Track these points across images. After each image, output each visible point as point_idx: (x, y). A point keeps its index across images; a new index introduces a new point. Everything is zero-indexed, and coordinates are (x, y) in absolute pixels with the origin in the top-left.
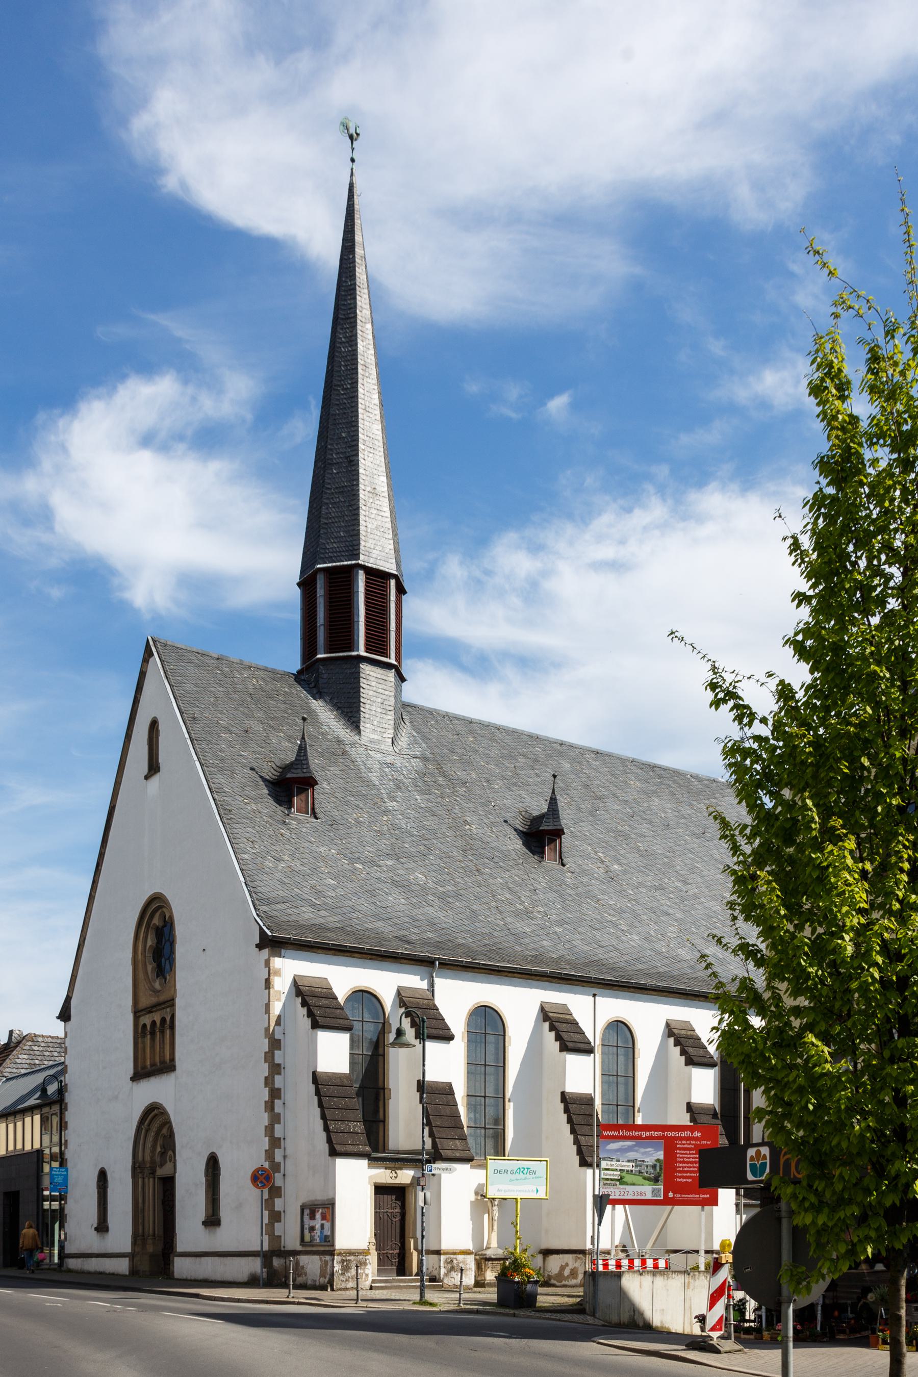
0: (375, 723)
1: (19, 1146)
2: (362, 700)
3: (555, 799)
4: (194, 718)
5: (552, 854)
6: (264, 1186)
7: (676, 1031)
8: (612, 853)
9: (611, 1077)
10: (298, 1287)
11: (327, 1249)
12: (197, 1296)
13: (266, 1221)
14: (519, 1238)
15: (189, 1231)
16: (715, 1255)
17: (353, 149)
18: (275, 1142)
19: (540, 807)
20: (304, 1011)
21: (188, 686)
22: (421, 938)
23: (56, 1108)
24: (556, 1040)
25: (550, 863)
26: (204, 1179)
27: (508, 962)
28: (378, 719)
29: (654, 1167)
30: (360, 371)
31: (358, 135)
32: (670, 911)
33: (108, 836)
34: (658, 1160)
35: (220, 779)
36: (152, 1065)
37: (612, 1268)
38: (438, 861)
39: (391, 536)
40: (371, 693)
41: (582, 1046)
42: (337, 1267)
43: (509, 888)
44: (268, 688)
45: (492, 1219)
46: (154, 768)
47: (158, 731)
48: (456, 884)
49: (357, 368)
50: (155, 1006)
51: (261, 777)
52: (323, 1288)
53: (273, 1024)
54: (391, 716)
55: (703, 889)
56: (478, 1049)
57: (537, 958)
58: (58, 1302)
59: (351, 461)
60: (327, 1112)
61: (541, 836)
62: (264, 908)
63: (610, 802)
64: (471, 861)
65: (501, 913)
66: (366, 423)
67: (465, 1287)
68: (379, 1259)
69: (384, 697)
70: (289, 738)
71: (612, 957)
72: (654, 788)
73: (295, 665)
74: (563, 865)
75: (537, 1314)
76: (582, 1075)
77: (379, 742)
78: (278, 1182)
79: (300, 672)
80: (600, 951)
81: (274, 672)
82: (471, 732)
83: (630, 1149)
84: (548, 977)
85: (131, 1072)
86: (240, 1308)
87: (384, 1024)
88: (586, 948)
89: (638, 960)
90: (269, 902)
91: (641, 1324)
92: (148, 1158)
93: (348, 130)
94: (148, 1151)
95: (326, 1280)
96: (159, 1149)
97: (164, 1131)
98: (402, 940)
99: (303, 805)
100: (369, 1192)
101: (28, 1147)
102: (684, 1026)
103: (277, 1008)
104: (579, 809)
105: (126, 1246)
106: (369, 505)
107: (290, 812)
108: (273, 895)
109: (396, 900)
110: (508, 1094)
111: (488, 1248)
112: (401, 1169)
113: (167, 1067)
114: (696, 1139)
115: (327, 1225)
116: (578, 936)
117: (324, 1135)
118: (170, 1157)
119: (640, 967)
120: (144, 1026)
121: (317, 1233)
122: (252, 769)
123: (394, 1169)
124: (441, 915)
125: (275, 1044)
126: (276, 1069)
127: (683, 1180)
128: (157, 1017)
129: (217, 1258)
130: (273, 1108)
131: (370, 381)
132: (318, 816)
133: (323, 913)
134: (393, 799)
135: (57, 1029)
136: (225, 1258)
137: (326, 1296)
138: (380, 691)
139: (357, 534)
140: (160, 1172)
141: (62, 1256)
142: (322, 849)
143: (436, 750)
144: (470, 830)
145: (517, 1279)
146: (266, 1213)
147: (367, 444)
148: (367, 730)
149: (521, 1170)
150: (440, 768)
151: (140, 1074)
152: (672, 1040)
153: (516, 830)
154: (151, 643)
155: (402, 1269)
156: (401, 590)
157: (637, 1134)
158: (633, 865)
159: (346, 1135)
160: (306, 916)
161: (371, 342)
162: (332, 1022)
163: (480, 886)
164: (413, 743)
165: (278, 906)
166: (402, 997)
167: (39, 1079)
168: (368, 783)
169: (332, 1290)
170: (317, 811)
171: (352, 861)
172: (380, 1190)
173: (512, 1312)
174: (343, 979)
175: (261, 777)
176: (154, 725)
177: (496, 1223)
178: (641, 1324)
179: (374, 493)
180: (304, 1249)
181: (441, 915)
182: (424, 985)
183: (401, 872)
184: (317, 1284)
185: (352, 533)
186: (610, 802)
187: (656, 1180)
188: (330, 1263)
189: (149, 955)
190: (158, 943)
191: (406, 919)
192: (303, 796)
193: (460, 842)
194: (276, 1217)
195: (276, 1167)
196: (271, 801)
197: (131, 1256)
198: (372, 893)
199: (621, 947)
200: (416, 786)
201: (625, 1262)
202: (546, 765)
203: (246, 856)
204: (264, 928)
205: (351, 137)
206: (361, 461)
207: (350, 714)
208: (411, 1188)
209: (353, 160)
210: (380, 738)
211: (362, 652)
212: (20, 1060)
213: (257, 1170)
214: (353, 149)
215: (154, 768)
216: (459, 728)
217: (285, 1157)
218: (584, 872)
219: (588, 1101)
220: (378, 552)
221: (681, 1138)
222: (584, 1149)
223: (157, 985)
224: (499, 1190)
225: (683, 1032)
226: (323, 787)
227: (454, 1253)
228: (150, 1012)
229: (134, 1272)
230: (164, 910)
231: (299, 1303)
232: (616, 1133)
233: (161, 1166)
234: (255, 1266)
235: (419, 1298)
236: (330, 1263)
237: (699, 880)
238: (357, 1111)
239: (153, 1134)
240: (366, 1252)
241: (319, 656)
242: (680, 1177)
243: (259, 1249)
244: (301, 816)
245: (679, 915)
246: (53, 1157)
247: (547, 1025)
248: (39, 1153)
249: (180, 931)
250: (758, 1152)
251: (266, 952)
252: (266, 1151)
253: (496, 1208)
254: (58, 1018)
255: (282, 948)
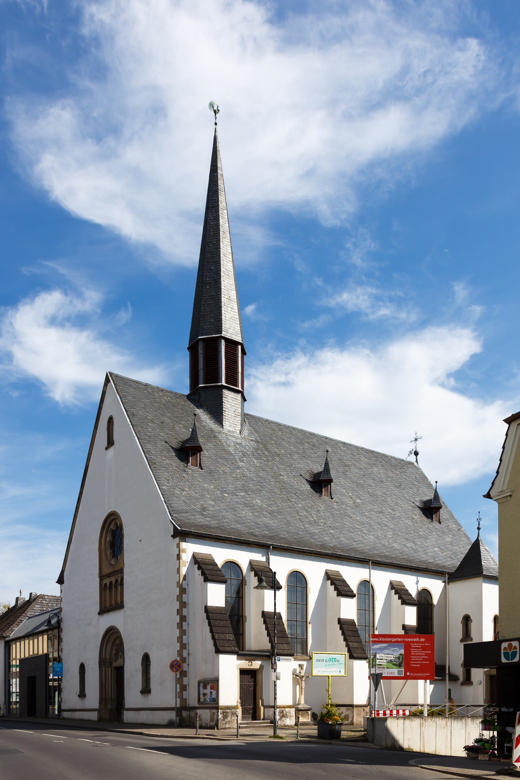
0: (231, 422)
1: (36, 652)
2: (224, 409)
3: (328, 463)
4: (134, 414)
5: (326, 493)
6: (177, 671)
7: (395, 586)
8: (356, 494)
9: (362, 611)
10: (201, 727)
11: (214, 706)
12: (141, 734)
13: (178, 690)
14: (331, 699)
15: (132, 695)
16: (420, 708)
17: (216, 118)
18: (183, 646)
19: (319, 468)
20: (200, 572)
21: (130, 398)
22: (260, 534)
23: (56, 632)
24: (335, 590)
25: (325, 497)
26: (141, 667)
27: (308, 547)
28: (232, 420)
29: (399, 658)
30: (221, 234)
31: (218, 110)
32: (388, 524)
33: (85, 482)
34: (401, 654)
35: (149, 446)
36: (110, 606)
37: (381, 715)
38: (268, 494)
39: (238, 323)
40: (229, 405)
41: (349, 593)
42: (220, 716)
43: (305, 509)
44: (173, 401)
45: (301, 688)
46: (110, 443)
47: (113, 423)
48: (278, 506)
49: (219, 233)
50: (112, 573)
51: (171, 446)
52: (212, 728)
53: (181, 579)
54: (239, 418)
55: (403, 514)
56: (292, 595)
57: (323, 546)
58: (61, 739)
59: (217, 282)
60: (213, 628)
61: (320, 483)
62: (176, 515)
63: (352, 468)
64: (285, 494)
65: (302, 522)
66: (225, 262)
67: (292, 726)
68: (242, 711)
69: (236, 408)
70: (186, 428)
71: (360, 546)
72: (374, 462)
73: (187, 392)
74: (332, 499)
75: (343, 743)
76: (349, 609)
77: (233, 432)
78: (185, 668)
79: (189, 395)
80: (354, 543)
81: (175, 394)
82: (280, 430)
83: (385, 648)
84: (330, 556)
85: (98, 610)
86: (171, 742)
87: (242, 580)
88: (347, 542)
89: (374, 548)
90: (178, 512)
91: (398, 747)
92: (108, 657)
93: (213, 107)
94: (108, 653)
95: (214, 723)
96: (114, 652)
97: (117, 642)
98: (251, 535)
99: (195, 462)
100: (237, 674)
101: (40, 653)
102: (399, 584)
103: (184, 570)
104: (337, 471)
105: (96, 705)
106: (227, 305)
107: (188, 465)
108: (180, 508)
109: (247, 514)
110: (309, 620)
111: (299, 704)
112: (254, 660)
113: (119, 606)
114: (422, 642)
115: (214, 692)
116: (342, 535)
117: (212, 642)
118: (121, 655)
119: (376, 552)
120: (106, 584)
121: (208, 697)
122: (166, 442)
123: (250, 660)
124: (271, 522)
125: (183, 591)
126: (183, 605)
127: (415, 666)
128: (113, 579)
129: (149, 711)
130: (182, 627)
131: (226, 240)
132: (203, 468)
133: (208, 519)
134: (242, 461)
135: (55, 590)
136: (153, 712)
137: (215, 732)
138: (233, 404)
139: (221, 320)
140: (115, 664)
141: (60, 710)
142: (206, 485)
143: (263, 438)
144: (283, 479)
145: (330, 723)
146: (178, 686)
147: (225, 273)
148: (227, 425)
149: (331, 660)
150: (265, 447)
151: (103, 611)
152: (393, 591)
153: (306, 480)
154: (109, 375)
155: (255, 716)
156: (244, 353)
157: (389, 639)
158: (367, 500)
159: (225, 642)
160: (199, 520)
161: (227, 220)
162: (213, 578)
163: (290, 508)
164: (251, 433)
165: (184, 515)
166: (252, 566)
167: (46, 617)
168: (229, 453)
169: (218, 729)
170: (202, 465)
171: (222, 492)
172: (243, 672)
173: (329, 742)
174: (220, 555)
175: (171, 446)
176: (111, 420)
177: (303, 690)
178: (398, 747)
179: (229, 298)
180: (200, 706)
181: (271, 522)
182: (264, 559)
183: (248, 499)
184: (208, 725)
185: (218, 320)
186: (352, 468)
187: (400, 666)
188: (216, 714)
189: (108, 546)
190: (113, 539)
191: (253, 524)
192: (194, 457)
193: (278, 485)
194: (184, 688)
195: (184, 660)
196: (176, 459)
197: (99, 710)
198: (234, 509)
199: (365, 541)
200: (254, 455)
201: (388, 712)
202: (319, 448)
203: (164, 487)
204: (176, 526)
205: (215, 111)
206: (222, 282)
207: (217, 417)
208: (259, 671)
209: (216, 124)
210: (233, 430)
211: (224, 383)
212: (37, 607)
213: (173, 662)
214: (216, 118)
215: (110, 443)
216: (274, 427)
217: (189, 654)
218: (343, 503)
219: (351, 623)
220: (231, 331)
221: (414, 642)
222: (352, 649)
223: (113, 562)
224: (319, 671)
225: (399, 587)
226: (205, 453)
227: (284, 707)
228: (109, 577)
229: (100, 719)
230: (116, 520)
231: (203, 738)
232: (377, 639)
233: (115, 661)
234: (172, 716)
235: (273, 734)
236: (216, 714)
237: (400, 509)
238: (228, 628)
239: (111, 643)
240: (236, 707)
241: (200, 385)
242: (413, 664)
243: (175, 706)
244: (194, 468)
245: (392, 526)
246: (55, 659)
247: (329, 582)
248: (47, 655)
249: (126, 531)
250: (510, 646)
251: (177, 540)
252: (178, 651)
253: (303, 682)
254: (57, 582)
255: (186, 537)
